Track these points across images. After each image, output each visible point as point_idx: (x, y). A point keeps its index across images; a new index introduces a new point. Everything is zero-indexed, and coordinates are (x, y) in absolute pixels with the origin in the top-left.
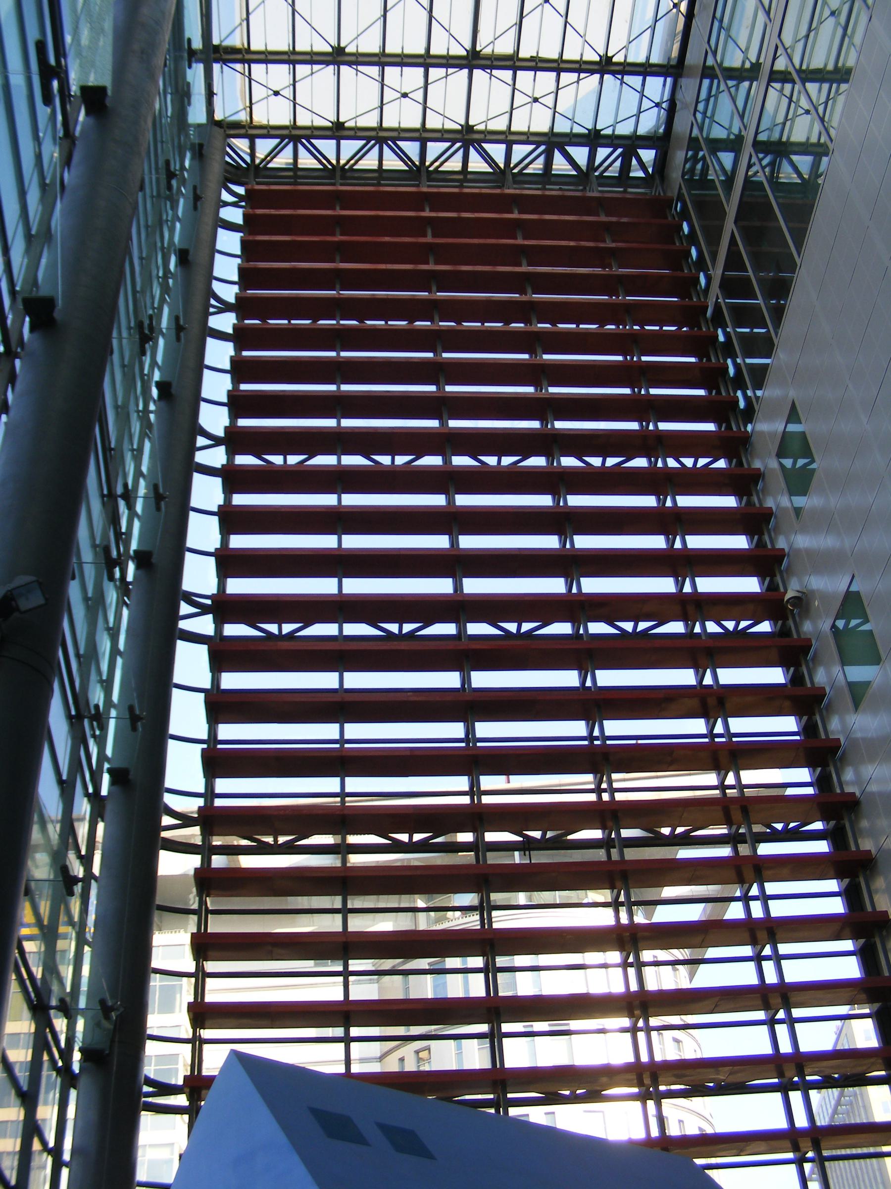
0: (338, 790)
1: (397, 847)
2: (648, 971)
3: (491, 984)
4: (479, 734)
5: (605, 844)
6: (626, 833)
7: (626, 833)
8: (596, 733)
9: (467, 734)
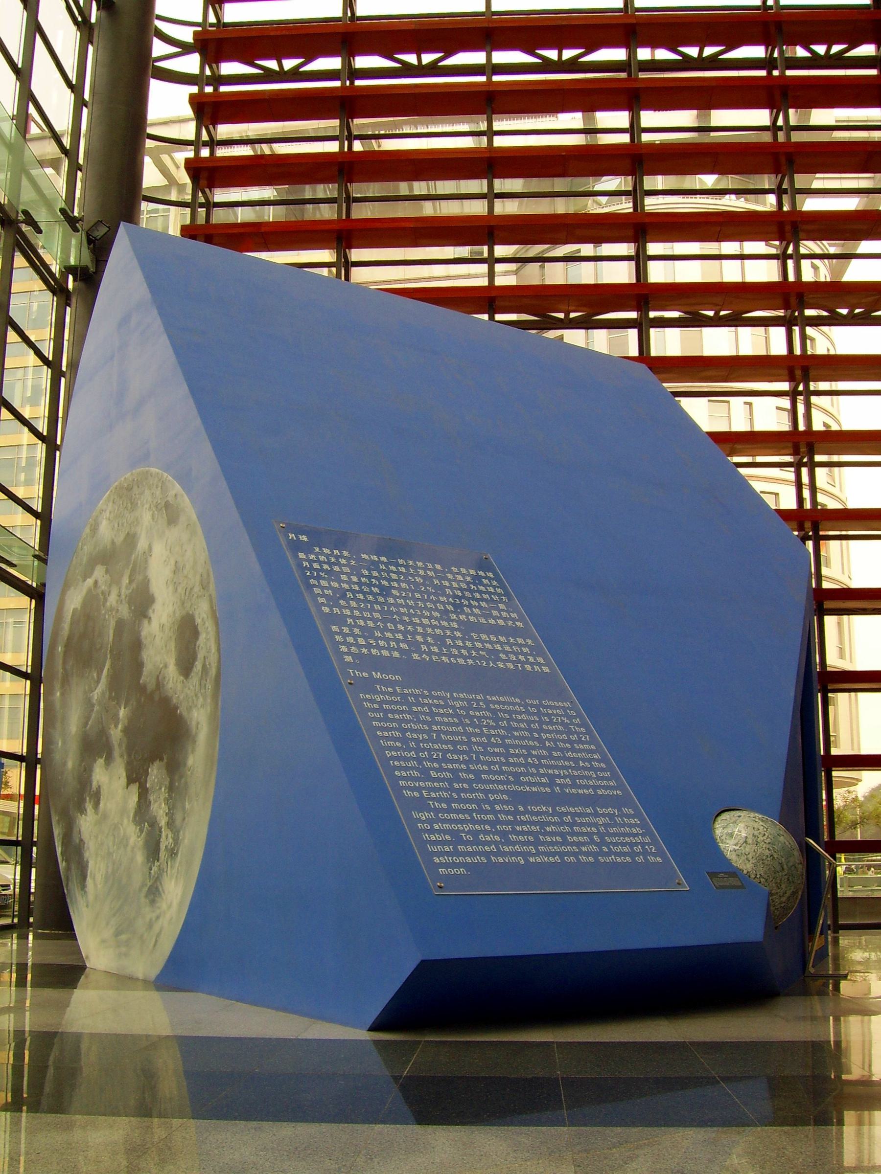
0: (485, 190)
1: (547, 66)
2: (805, 264)
3: (635, 120)
4: (644, 124)
5: (767, 63)
6: (809, 312)
7: (809, 312)
8: (780, 122)
9: (632, 125)
